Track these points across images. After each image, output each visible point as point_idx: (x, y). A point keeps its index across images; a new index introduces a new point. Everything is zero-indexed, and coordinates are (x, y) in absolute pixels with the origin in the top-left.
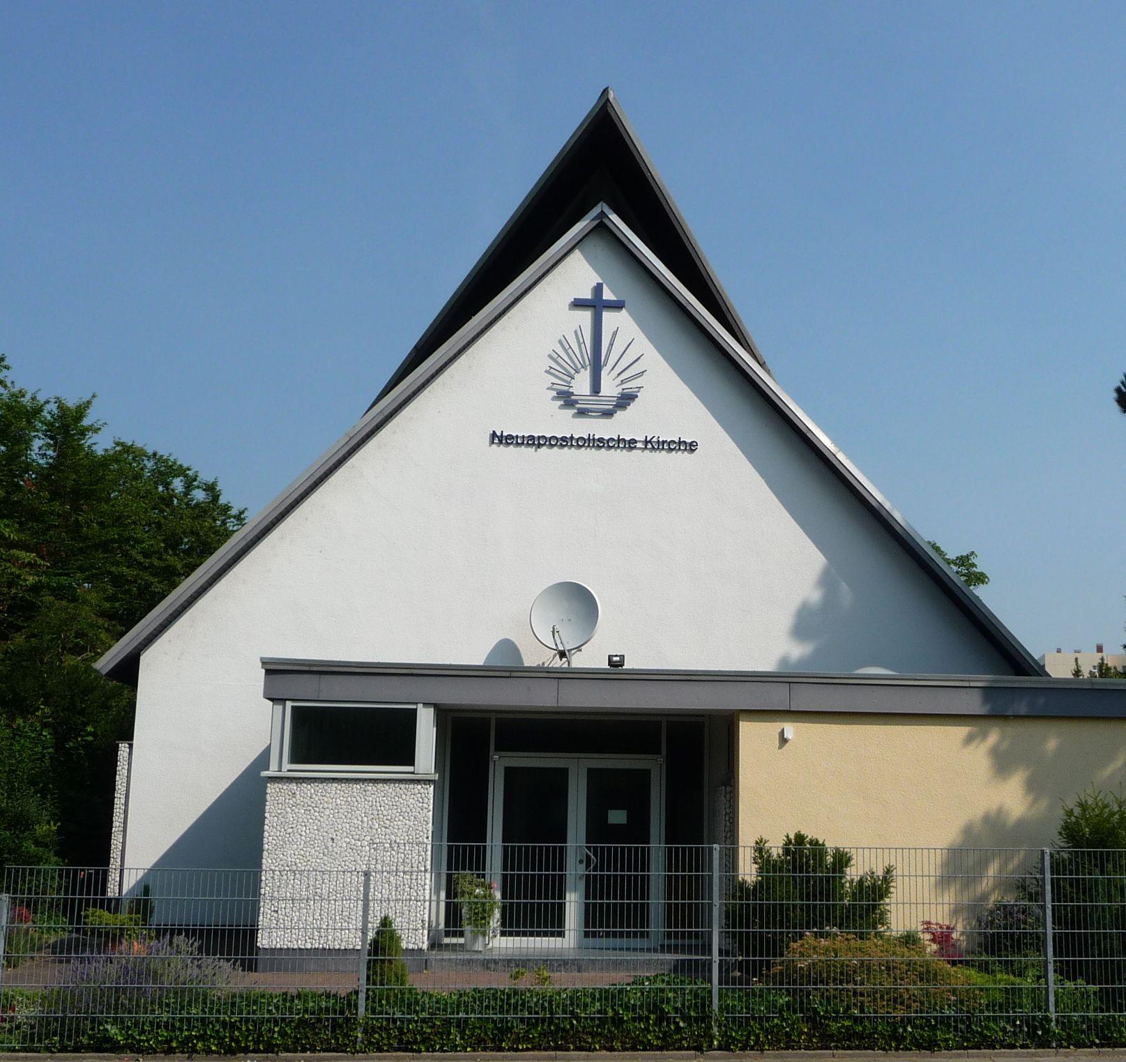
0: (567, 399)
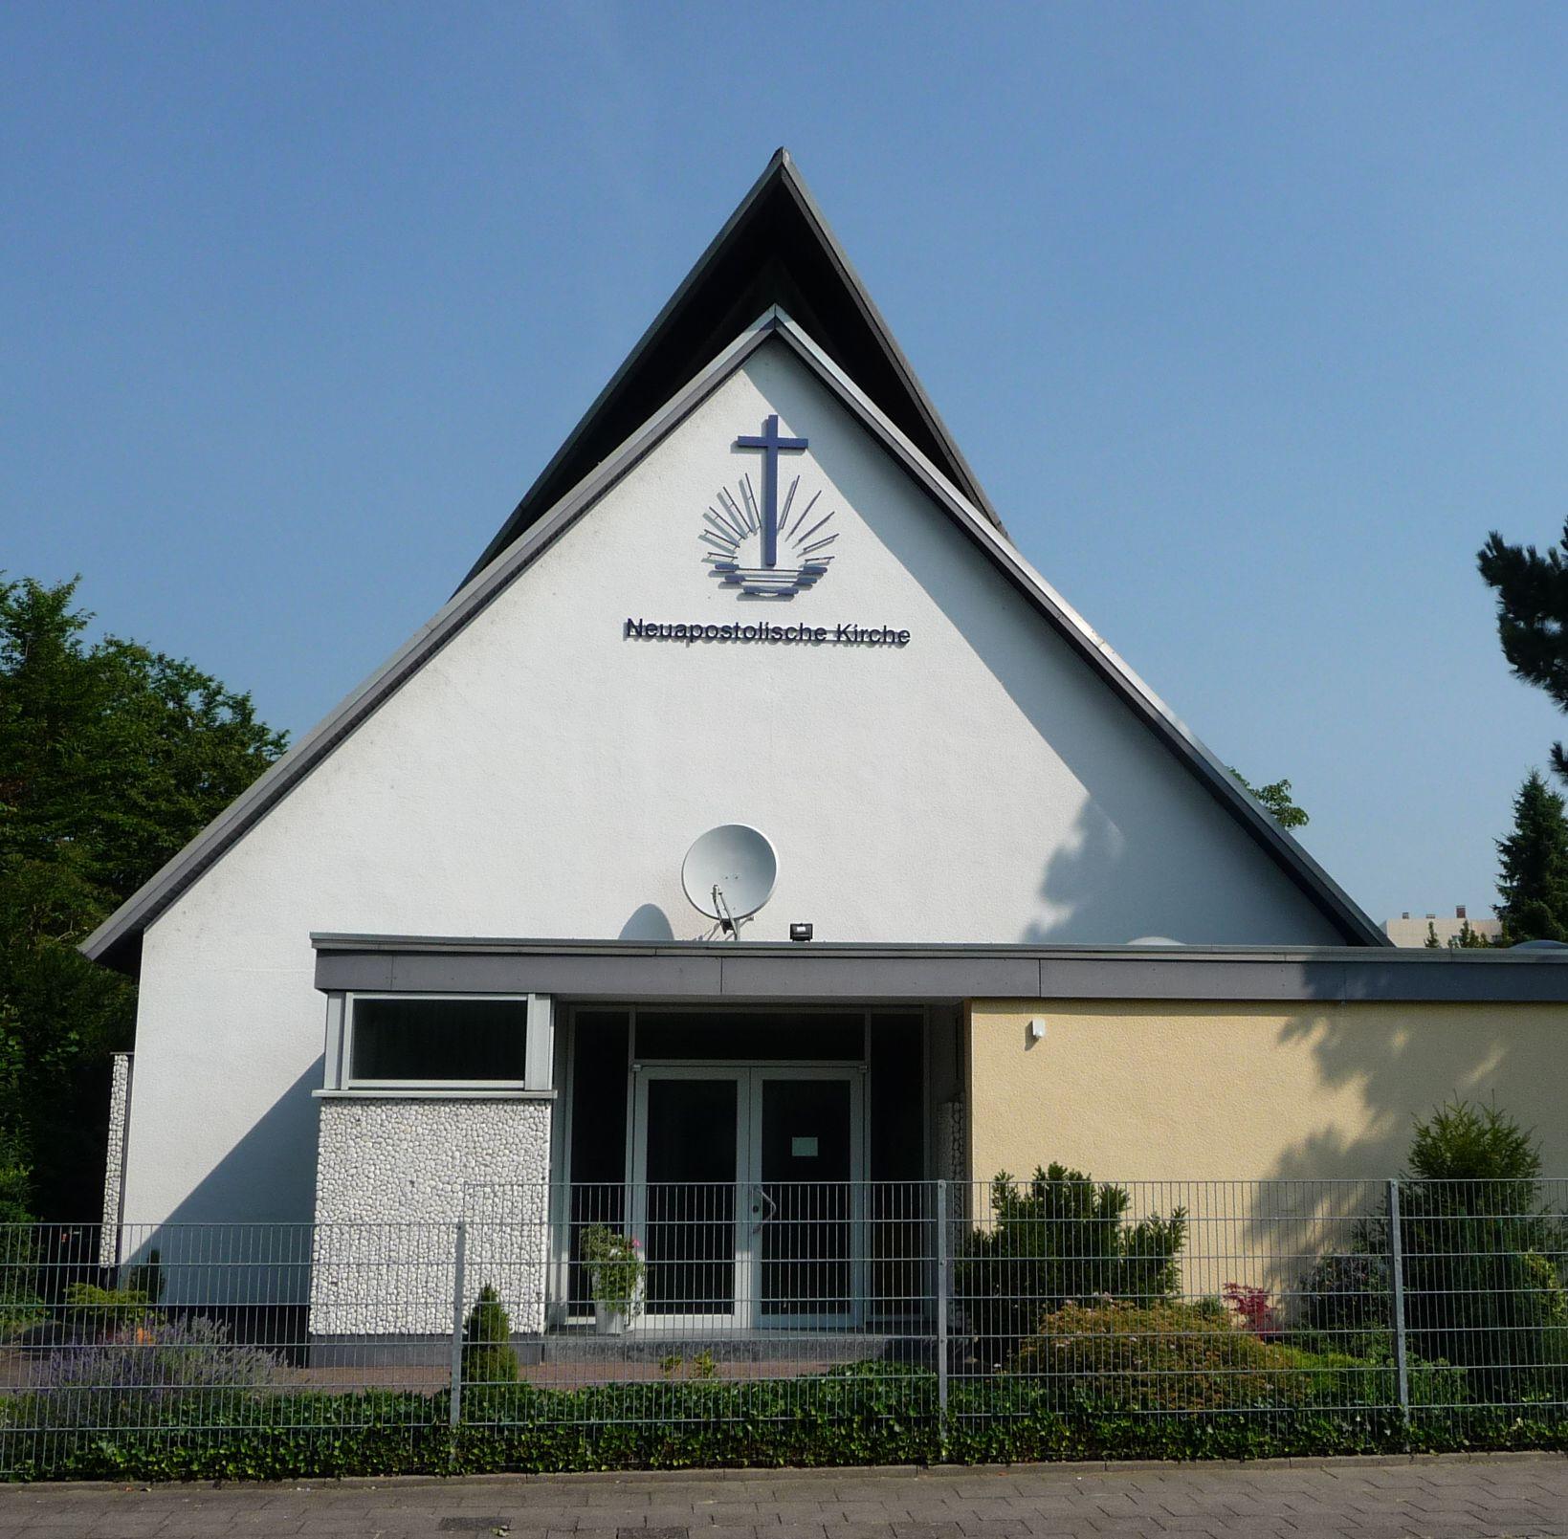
0: (729, 574)
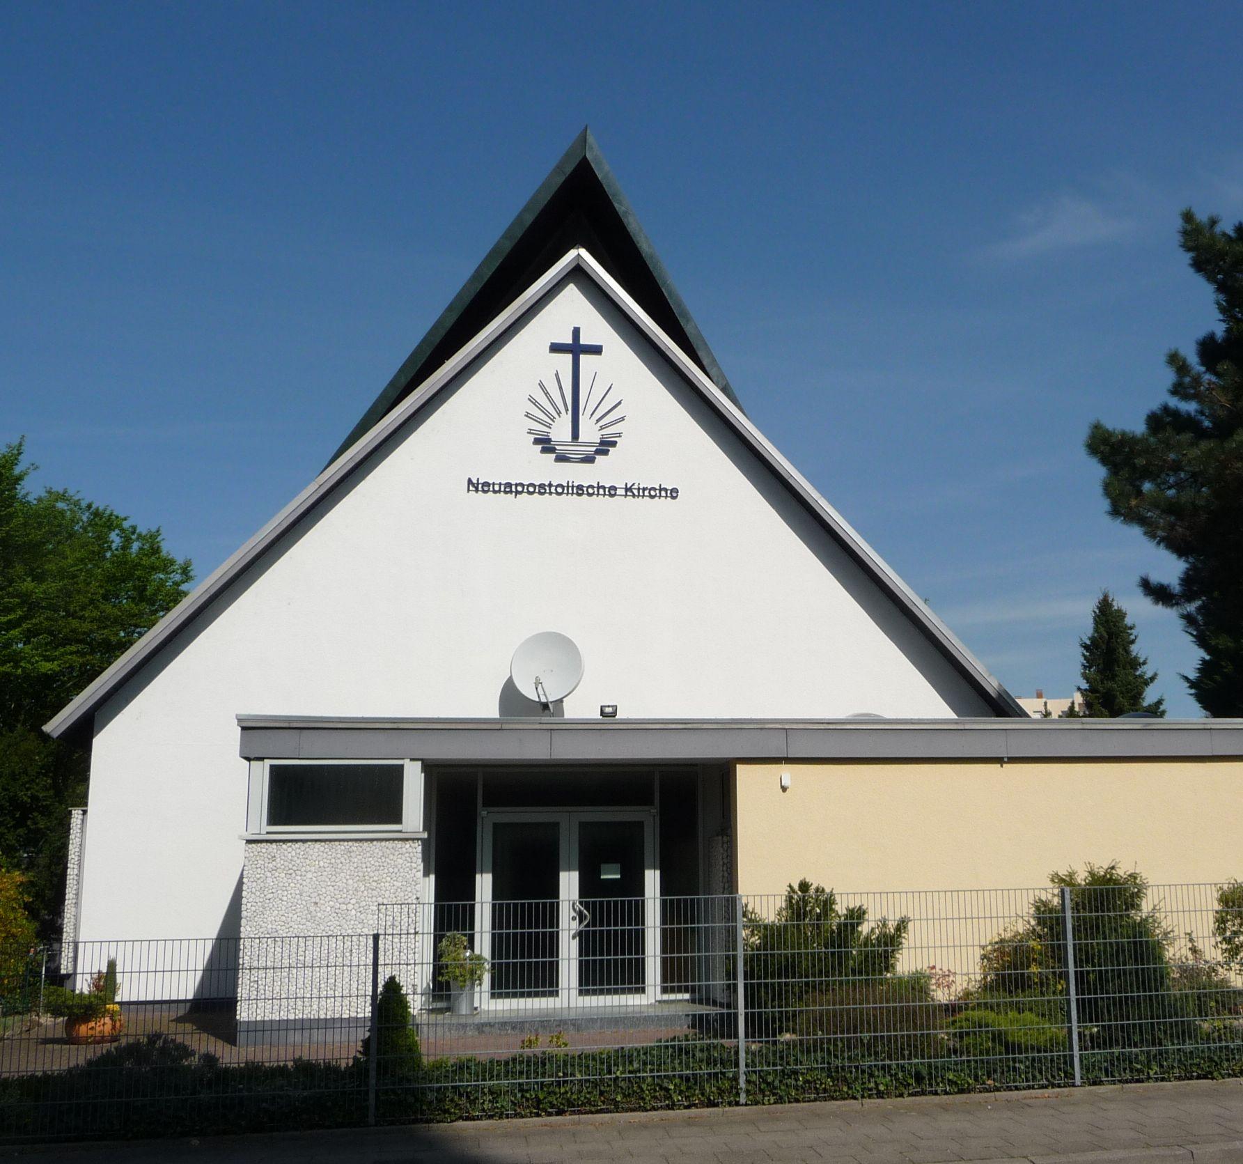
0: (545, 444)
